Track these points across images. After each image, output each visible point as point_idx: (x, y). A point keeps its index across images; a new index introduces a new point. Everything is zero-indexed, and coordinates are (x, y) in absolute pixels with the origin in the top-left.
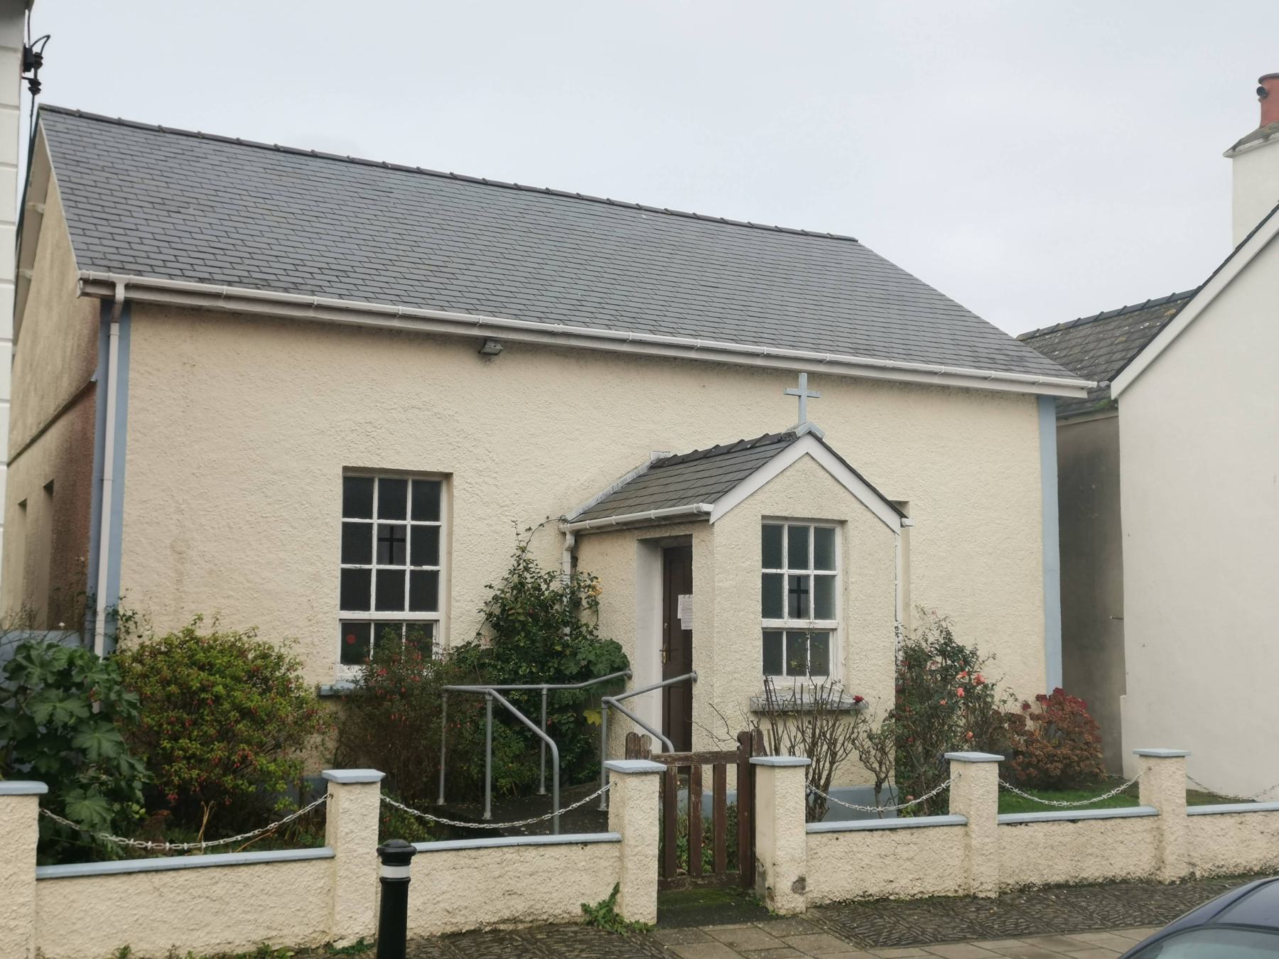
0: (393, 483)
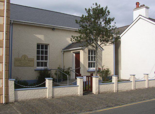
0: (42, 46)
